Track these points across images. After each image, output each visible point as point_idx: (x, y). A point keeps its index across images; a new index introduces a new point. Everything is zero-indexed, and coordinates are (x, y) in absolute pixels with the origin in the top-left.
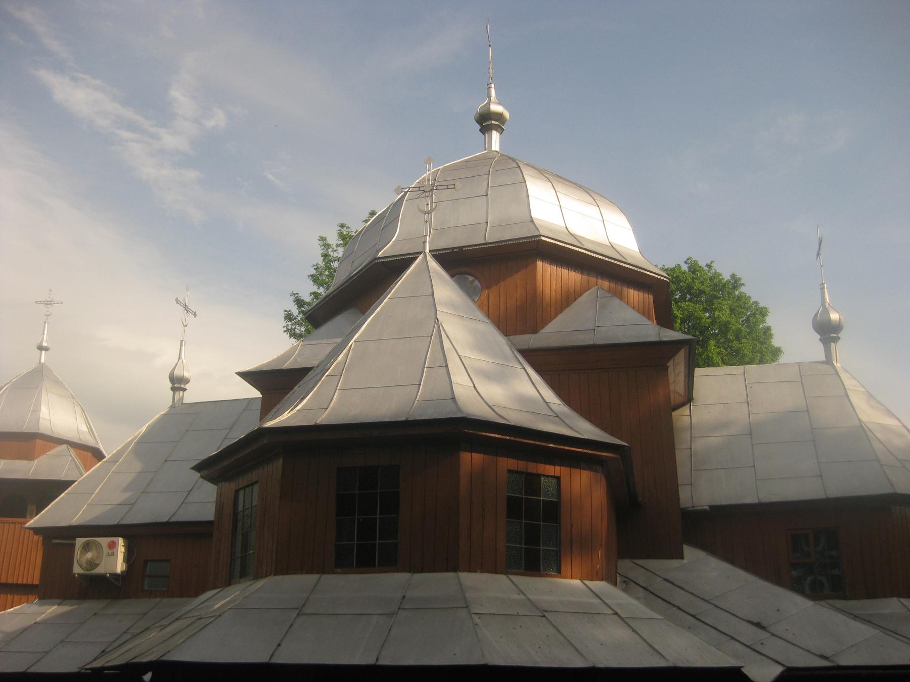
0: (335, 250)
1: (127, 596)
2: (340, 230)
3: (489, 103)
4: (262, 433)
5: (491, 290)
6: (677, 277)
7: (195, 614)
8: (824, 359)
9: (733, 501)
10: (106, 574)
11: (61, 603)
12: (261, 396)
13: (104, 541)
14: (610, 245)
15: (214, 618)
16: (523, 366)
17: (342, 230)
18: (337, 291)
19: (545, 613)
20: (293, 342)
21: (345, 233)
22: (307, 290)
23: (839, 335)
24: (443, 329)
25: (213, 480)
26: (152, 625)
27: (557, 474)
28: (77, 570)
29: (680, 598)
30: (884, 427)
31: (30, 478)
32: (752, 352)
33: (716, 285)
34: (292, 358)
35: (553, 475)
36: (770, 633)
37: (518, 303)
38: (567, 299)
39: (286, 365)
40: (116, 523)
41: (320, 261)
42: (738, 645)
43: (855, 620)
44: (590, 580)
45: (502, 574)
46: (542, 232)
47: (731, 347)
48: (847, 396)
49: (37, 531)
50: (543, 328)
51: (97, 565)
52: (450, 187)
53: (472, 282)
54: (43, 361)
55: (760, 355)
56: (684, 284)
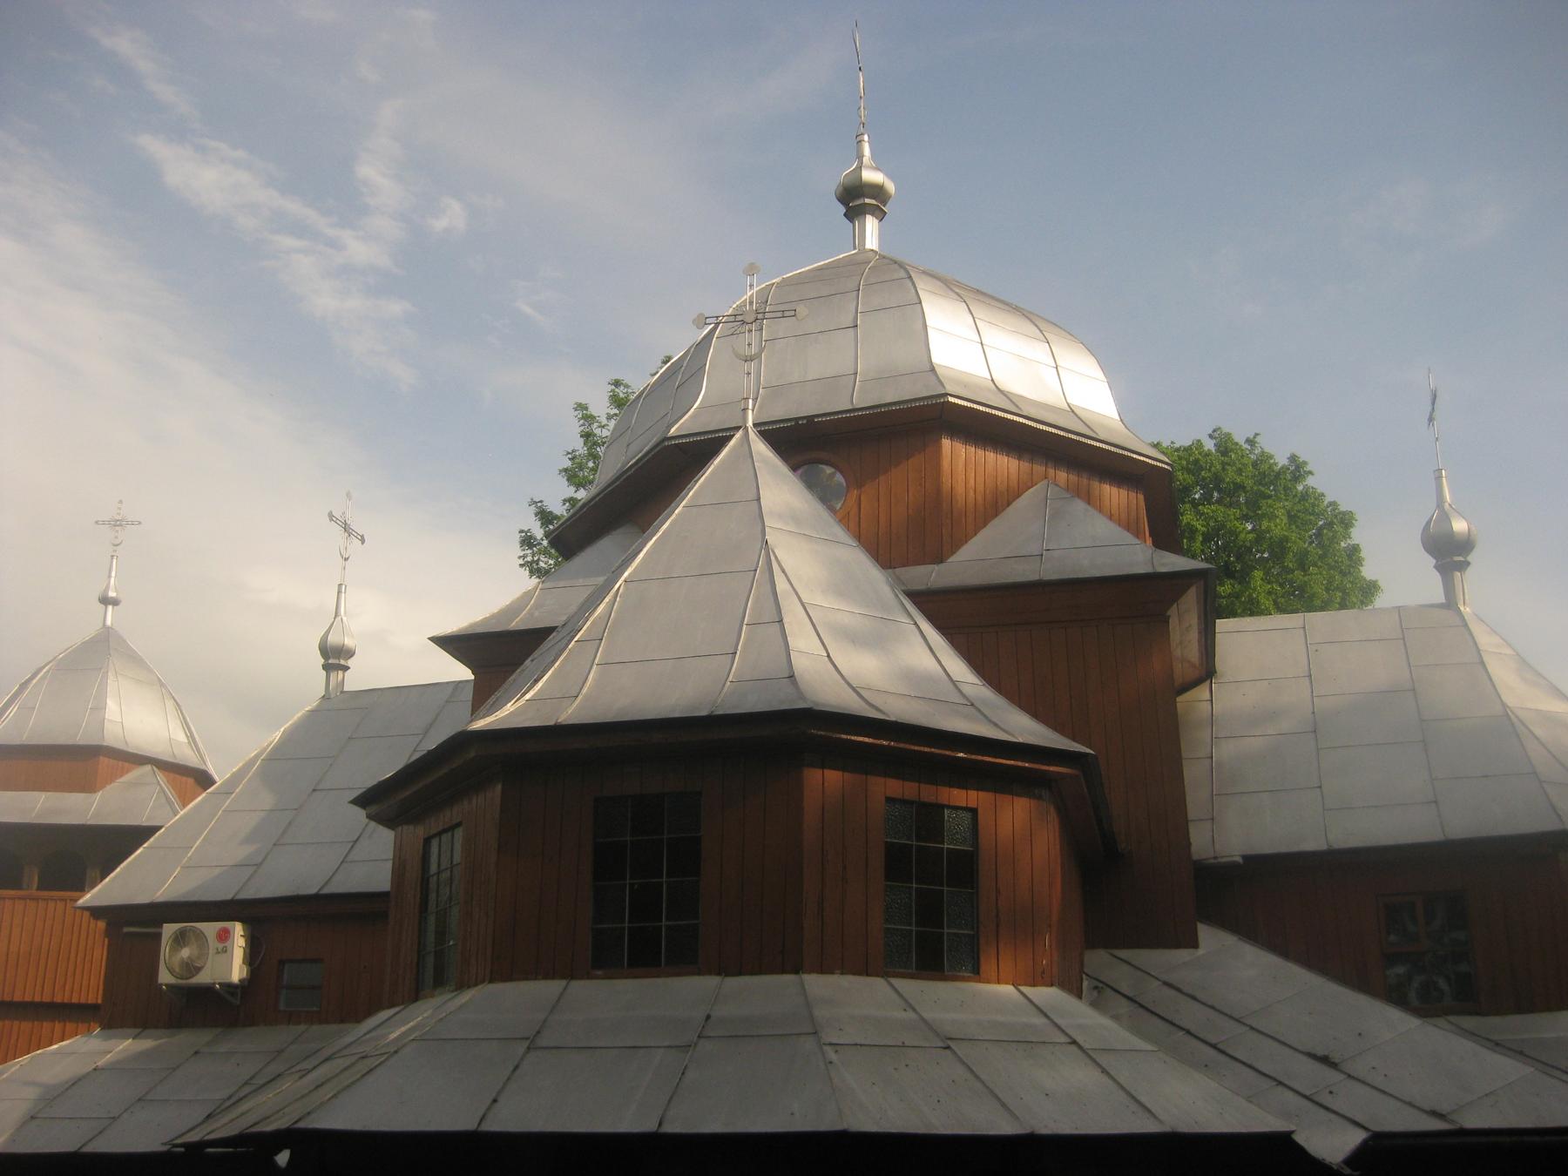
0: (603, 424)
1: (251, 1021)
2: (612, 391)
3: (860, 168)
4: (464, 740)
5: (863, 489)
6: (1196, 461)
7: (355, 1051)
8: (1442, 599)
9: (1283, 849)
10: (214, 984)
11: (139, 1034)
12: (473, 677)
13: (210, 929)
14: (1069, 409)
15: (386, 1056)
16: (913, 619)
17: (617, 390)
18: (602, 495)
19: (950, 1043)
20: (535, 580)
21: (622, 395)
22: (559, 496)
23: (1469, 558)
24: (776, 558)
25: (388, 821)
26: (286, 1071)
27: (972, 805)
28: (165, 977)
29: (1190, 1014)
30: (1547, 717)
31: (89, 823)
32: (1327, 590)
33: (1263, 475)
34: (524, 612)
35: (965, 805)
36: (1345, 1073)
37: (910, 511)
38: (996, 503)
39: (514, 624)
40: (229, 897)
41: (579, 446)
42: (1290, 1094)
43: (1495, 1051)
44: (1031, 986)
45: (877, 976)
46: (950, 389)
47: (1291, 582)
48: (1482, 663)
49: (96, 912)
50: (953, 553)
51: (199, 970)
52: (787, 314)
53: (832, 475)
54: (109, 622)
55: (1341, 594)
56: (1208, 475)
